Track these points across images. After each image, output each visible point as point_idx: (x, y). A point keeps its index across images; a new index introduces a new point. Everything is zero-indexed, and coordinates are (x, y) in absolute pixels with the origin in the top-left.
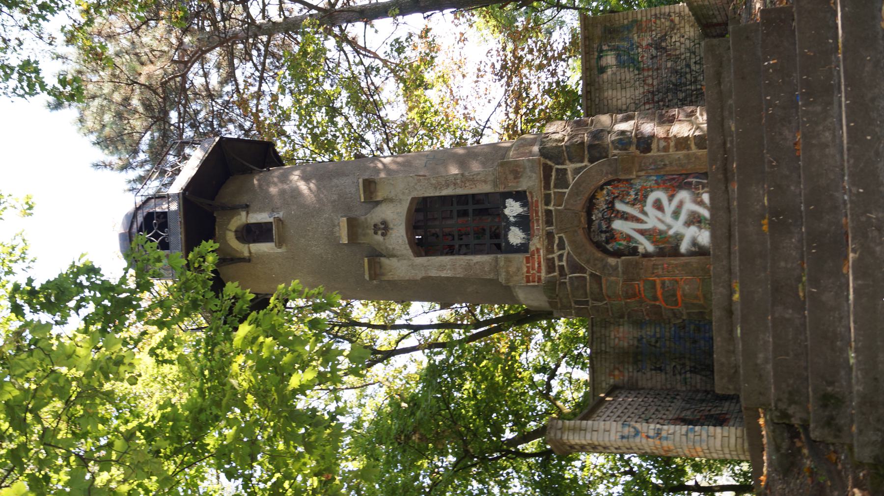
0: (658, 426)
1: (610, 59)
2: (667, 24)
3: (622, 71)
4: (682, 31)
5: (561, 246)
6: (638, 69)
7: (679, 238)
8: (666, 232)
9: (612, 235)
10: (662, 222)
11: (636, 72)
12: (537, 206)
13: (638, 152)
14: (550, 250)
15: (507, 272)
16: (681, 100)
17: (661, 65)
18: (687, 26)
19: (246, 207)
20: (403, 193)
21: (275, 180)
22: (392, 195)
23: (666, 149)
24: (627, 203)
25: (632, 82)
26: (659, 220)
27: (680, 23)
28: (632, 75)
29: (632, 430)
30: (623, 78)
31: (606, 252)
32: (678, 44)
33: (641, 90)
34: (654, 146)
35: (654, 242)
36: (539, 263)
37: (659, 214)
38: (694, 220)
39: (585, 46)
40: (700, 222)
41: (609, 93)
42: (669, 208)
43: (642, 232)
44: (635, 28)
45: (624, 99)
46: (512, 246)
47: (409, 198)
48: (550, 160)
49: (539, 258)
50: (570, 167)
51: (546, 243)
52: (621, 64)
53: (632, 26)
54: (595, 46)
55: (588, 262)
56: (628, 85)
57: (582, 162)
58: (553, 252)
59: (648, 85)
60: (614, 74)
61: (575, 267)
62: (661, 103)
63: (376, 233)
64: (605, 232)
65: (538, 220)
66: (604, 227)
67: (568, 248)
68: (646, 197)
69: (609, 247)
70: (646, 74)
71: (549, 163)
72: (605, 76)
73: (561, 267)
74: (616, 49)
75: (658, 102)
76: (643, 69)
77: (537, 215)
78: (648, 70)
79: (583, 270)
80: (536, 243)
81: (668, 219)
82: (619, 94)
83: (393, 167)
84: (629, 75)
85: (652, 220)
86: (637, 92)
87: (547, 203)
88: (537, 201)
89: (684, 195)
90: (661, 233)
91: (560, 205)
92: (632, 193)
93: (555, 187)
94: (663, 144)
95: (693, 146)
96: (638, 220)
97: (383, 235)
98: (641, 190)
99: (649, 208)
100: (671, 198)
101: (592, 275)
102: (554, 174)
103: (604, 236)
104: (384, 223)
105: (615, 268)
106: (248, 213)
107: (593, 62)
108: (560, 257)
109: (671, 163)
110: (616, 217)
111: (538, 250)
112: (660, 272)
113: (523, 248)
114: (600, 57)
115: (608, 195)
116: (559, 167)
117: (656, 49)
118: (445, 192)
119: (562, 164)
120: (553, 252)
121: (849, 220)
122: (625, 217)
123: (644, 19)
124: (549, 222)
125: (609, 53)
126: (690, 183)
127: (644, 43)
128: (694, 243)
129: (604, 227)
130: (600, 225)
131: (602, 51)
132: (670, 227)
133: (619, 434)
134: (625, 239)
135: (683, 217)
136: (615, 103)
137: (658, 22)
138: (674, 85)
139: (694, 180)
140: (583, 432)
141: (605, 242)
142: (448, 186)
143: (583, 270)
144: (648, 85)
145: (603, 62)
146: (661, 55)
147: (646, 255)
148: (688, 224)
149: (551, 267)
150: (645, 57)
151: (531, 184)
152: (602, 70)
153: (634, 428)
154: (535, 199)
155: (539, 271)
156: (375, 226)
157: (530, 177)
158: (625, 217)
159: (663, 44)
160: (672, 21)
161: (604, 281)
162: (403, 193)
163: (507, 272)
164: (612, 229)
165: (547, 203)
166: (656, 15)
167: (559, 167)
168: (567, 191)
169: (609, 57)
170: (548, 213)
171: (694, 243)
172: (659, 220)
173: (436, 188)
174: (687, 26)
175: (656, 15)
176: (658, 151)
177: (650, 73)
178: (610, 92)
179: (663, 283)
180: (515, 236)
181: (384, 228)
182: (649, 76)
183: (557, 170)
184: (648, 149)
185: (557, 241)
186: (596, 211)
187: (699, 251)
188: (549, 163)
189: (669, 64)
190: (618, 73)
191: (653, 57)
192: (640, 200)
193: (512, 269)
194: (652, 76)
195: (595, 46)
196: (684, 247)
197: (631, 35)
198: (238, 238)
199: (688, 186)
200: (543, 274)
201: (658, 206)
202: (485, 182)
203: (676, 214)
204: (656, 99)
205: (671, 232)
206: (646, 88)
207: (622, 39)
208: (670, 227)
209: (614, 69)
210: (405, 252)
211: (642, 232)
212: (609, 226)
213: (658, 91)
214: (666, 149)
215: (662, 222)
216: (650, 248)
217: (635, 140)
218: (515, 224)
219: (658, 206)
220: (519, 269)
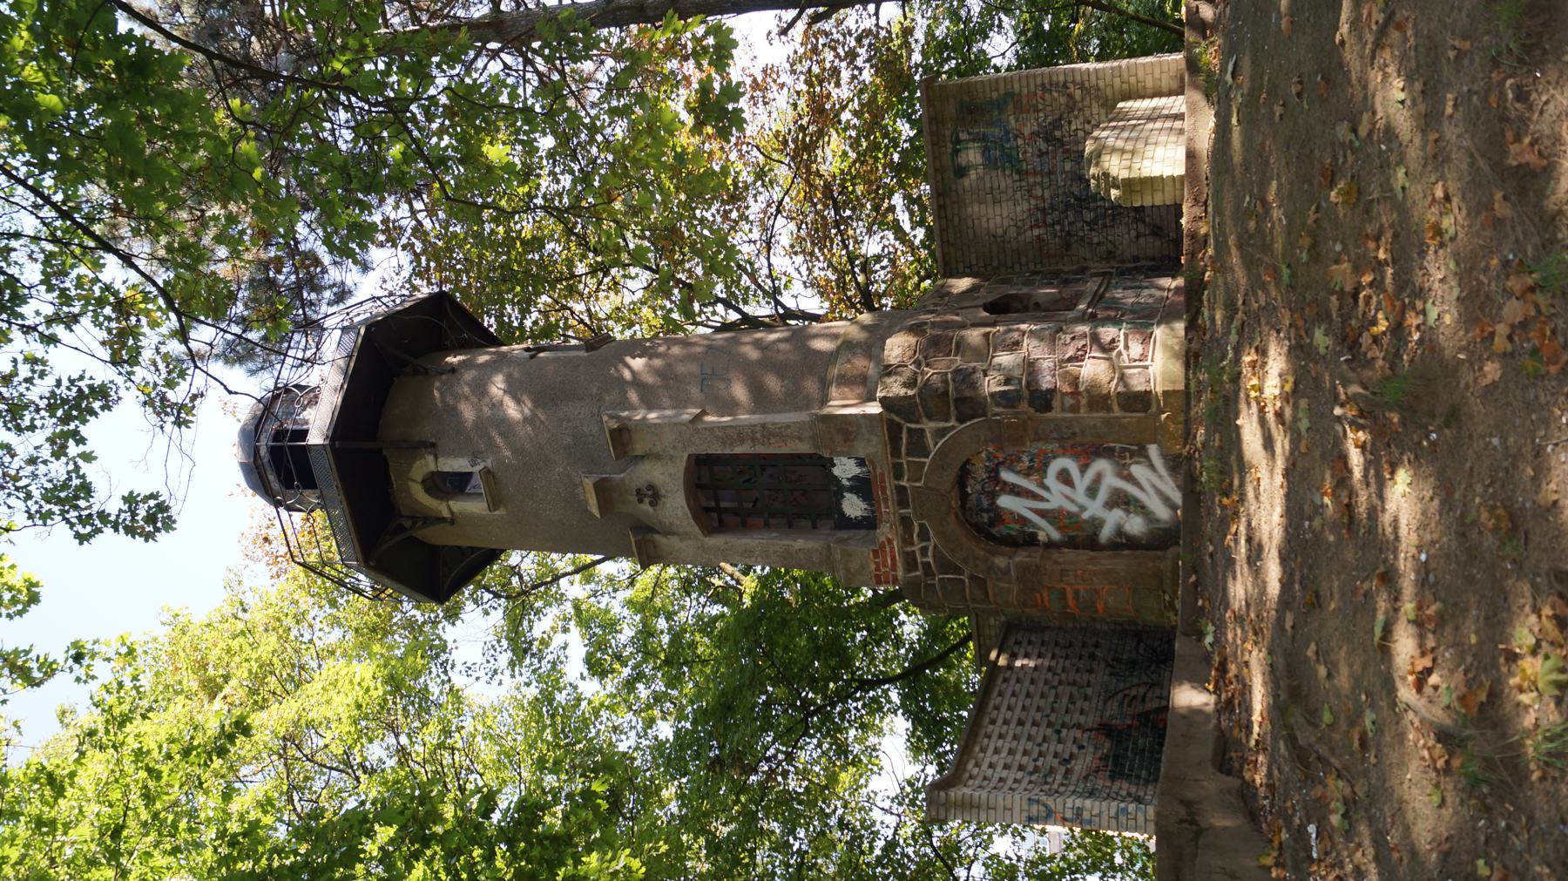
0: (1078, 802)
1: (972, 155)
2: (1063, 100)
3: (994, 174)
4: (1087, 113)
5: (924, 536)
6: (1019, 172)
7: (1097, 524)
8: (1077, 515)
9: (998, 515)
10: (1072, 501)
11: (1016, 177)
12: (883, 481)
13: (1032, 410)
14: (907, 540)
15: (847, 570)
16: (1088, 224)
17: (1054, 166)
18: (1095, 105)
19: (433, 447)
20: (675, 448)
21: (467, 389)
22: (659, 448)
23: (1074, 409)
24: (1018, 473)
25: (1010, 192)
26: (1067, 497)
27: (1083, 99)
28: (1009, 181)
29: (1042, 808)
30: (995, 185)
31: (990, 537)
32: (1081, 134)
33: (1026, 206)
34: (1056, 403)
35: (1059, 528)
36: (893, 559)
37: (1067, 490)
38: (1120, 500)
39: (931, 133)
40: (1127, 503)
41: (974, 209)
42: (1081, 483)
43: (1042, 513)
44: (1011, 107)
45: (998, 219)
46: (849, 519)
47: (686, 456)
48: (897, 414)
49: (892, 549)
50: (929, 426)
51: (900, 531)
52: (990, 163)
53: (1006, 103)
54: (948, 133)
55: (965, 561)
56: (1004, 197)
57: (947, 421)
58: (912, 544)
59: (1036, 198)
60: (981, 178)
61: (946, 566)
62: (1058, 228)
63: (640, 501)
64: (987, 511)
65: (886, 500)
66: (985, 503)
67: (934, 540)
68: (1046, 465)
69: (994, 531)
70: (1031, 180)
71: (896, 419)
72: (966, 182)
73: (926, 565)
74: (982, 138)
75: (1052, 225)
76: (1027, 173)
77: (884, 492)
78: (1035, 174)
79: (958, 571)
80: (888, 510)
81: (1080, 497)
82: (990, 211)
83: (649, 379)
84: (1004, 181)
85: (1057, 496)
86: (1019, 209)
87: (898, 475)
88: (882, 474)
89: (1102, 465)
90: (1070, 515)
91: (918, 480)
92: (1025, 458)
93: (908, 454)
94: (1069, 401)
95: (1116, 407)
96: (1042, 499)
97: (651, 504)
98: (1037, 455)
99: (1051, 480)
100: (1084, 469)
101: (972, 577)
102: (904, 436)
103: (985, 516)
104: (651, 487)
105: (1006, 572)
106: (436, 458)
107: (946, 159)
108: (924, 551)
109: (1083, 432)
110: (1003, 491)
111: (890, 541)
112: (1072, 579)
113: (868, 523)
114: (956, 152)
115: (989, 459)
116: (913, 426)
117: (1046, 140)
118: (738, 450)
119: (917, 422)
120: (912, 544)
121: (1342, 390)
122: (1016, 491)
123: (1025, 91)
124: (902, 502)
125: (971, 145)
126: (1113, 449)
127: (1027, 131)
128: (1119, 531)
129: (985, 503)
130: (979, 500)
131: (958, 141)
132: (1083, 509)
133: (1025, 814)
134: (1017, 522)
135: (1103, 495)
136: (984, 224)
137: (1047, 96)
138: (1076, 198)
139: (1118, 446)
140: (975, 811)
141: (993, 531)
142: (742, 441)
143: (958, 571)
144: (1036, 198)
145: (963, 159)
146: (1055, 152)
147: (1050, 545)
148: (1110, 505)
149: (911, 563)
150: (1028, 152)
151: (871, 450)
152: (961, 172)
153: (1046, 806)
154: (879, 471)
155: (894, 567)
156: (638, 491)
157: (869, 441)
158: (1016, 491)
159: (1058, 133)
160: (1070, 96)
161: (989, 584)
162: (675, 448)
163: (847, 570)
164: (998, 507)
165: (898, 476)
166: (1043, 85)
167: (913, 426)
168: (927, 461)
169: (971, 152)
170: (901, 490)
171: (1119, 531)
172: (1067, 497)
173: (724, 443)
174: (1095, 105)
175: (1043, 85)
176: (1063, 410)
177: (1039, 179)
178: (976, 208)
179: (1076, 593)
180: (853, 506)
181: (653, 494)
182: (1036, 184)
183: (909, 430)
184: (1049, 408)
185: (917, 530)
186: (972, 482)
187: (1124, 543)
188: (896, 419)
189: (1068, 166)
190: (987, 178)
191: (1042, 154)
192: (1038, 469)
193: (854, 566)
194: (1041, 184)
195: (948, 133)
196: (1106, 533)
197: (1004, 117)
198: (428, 491)
199: (1108, 453)
200: (900, 573)
201: (1064, 477)
202: (800, 439)
203: (1092, 492)
204: (1049, 220)
205: (1085, 516)
206: (1033, 202)
207: (991, 124)
208: (1083, 509)
209: (980, 170)
210: (689, 529)
211: (1042, 513)
212: (993, 503)
213: (1053, 208)
214: (1074, 409)
215: (1072, 501)
216: (1056, 535)
217: (1026, 394)
218: (851, 490)
219: (1064, 477)
220: (863, 567)
